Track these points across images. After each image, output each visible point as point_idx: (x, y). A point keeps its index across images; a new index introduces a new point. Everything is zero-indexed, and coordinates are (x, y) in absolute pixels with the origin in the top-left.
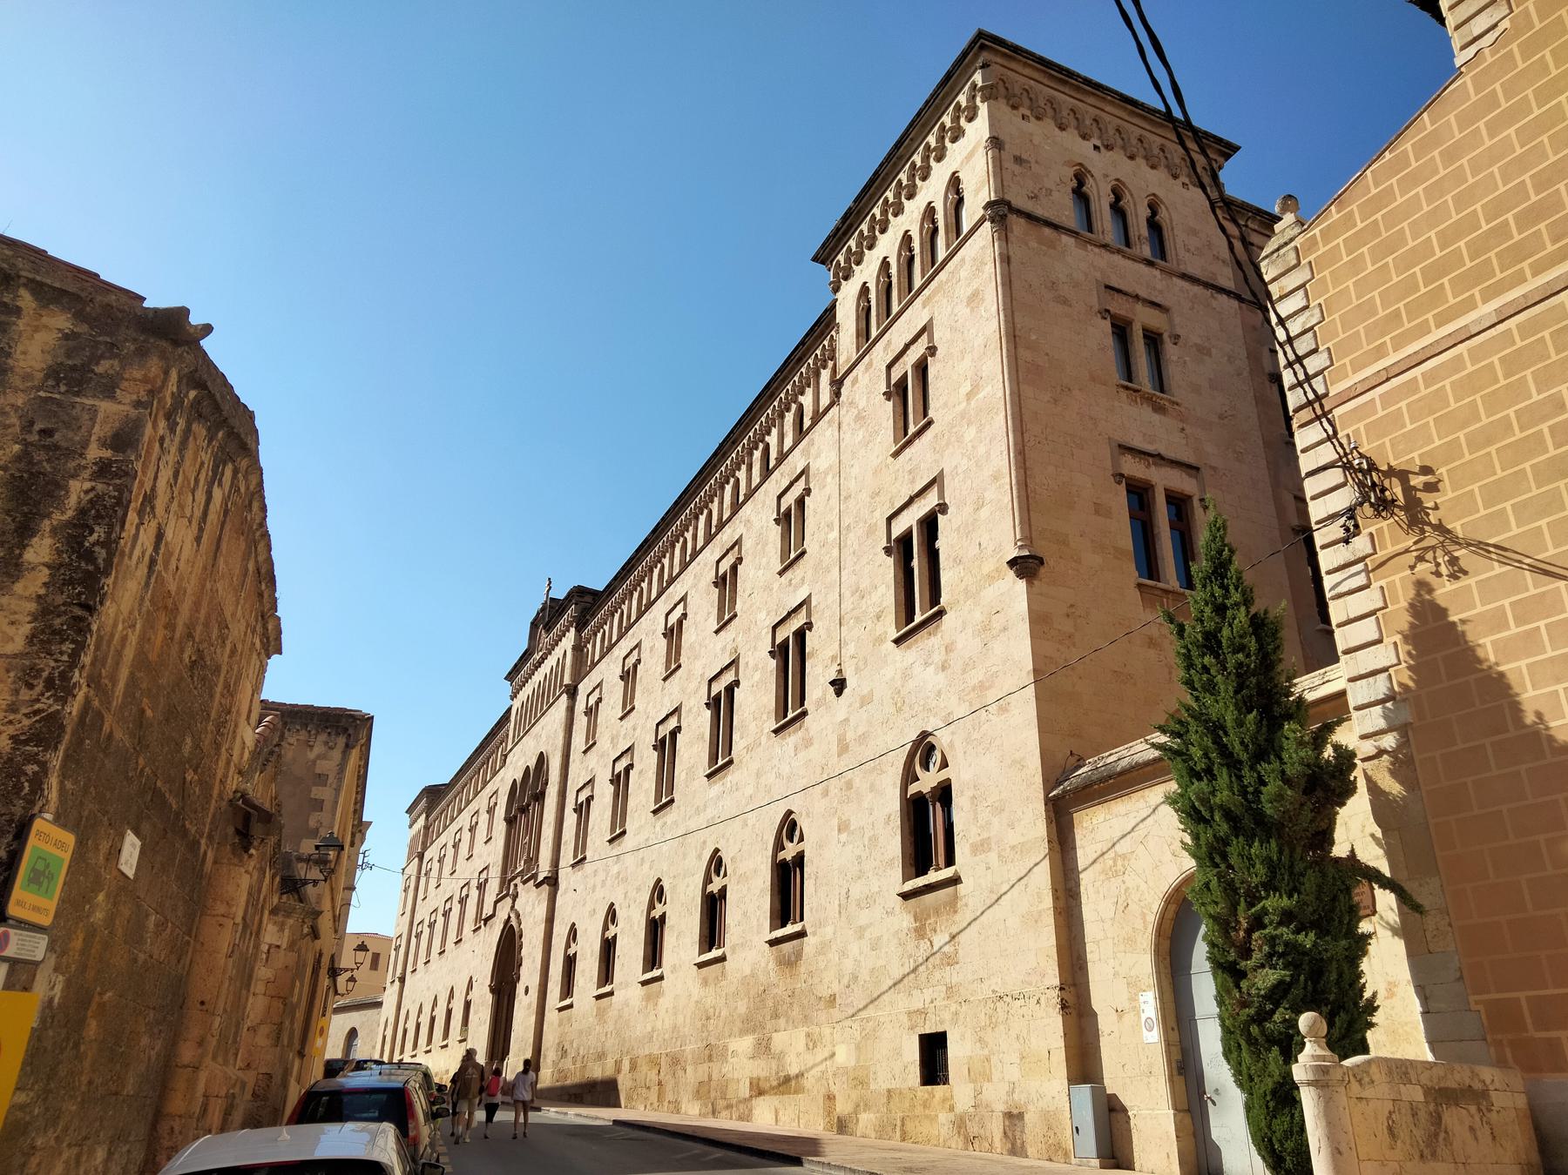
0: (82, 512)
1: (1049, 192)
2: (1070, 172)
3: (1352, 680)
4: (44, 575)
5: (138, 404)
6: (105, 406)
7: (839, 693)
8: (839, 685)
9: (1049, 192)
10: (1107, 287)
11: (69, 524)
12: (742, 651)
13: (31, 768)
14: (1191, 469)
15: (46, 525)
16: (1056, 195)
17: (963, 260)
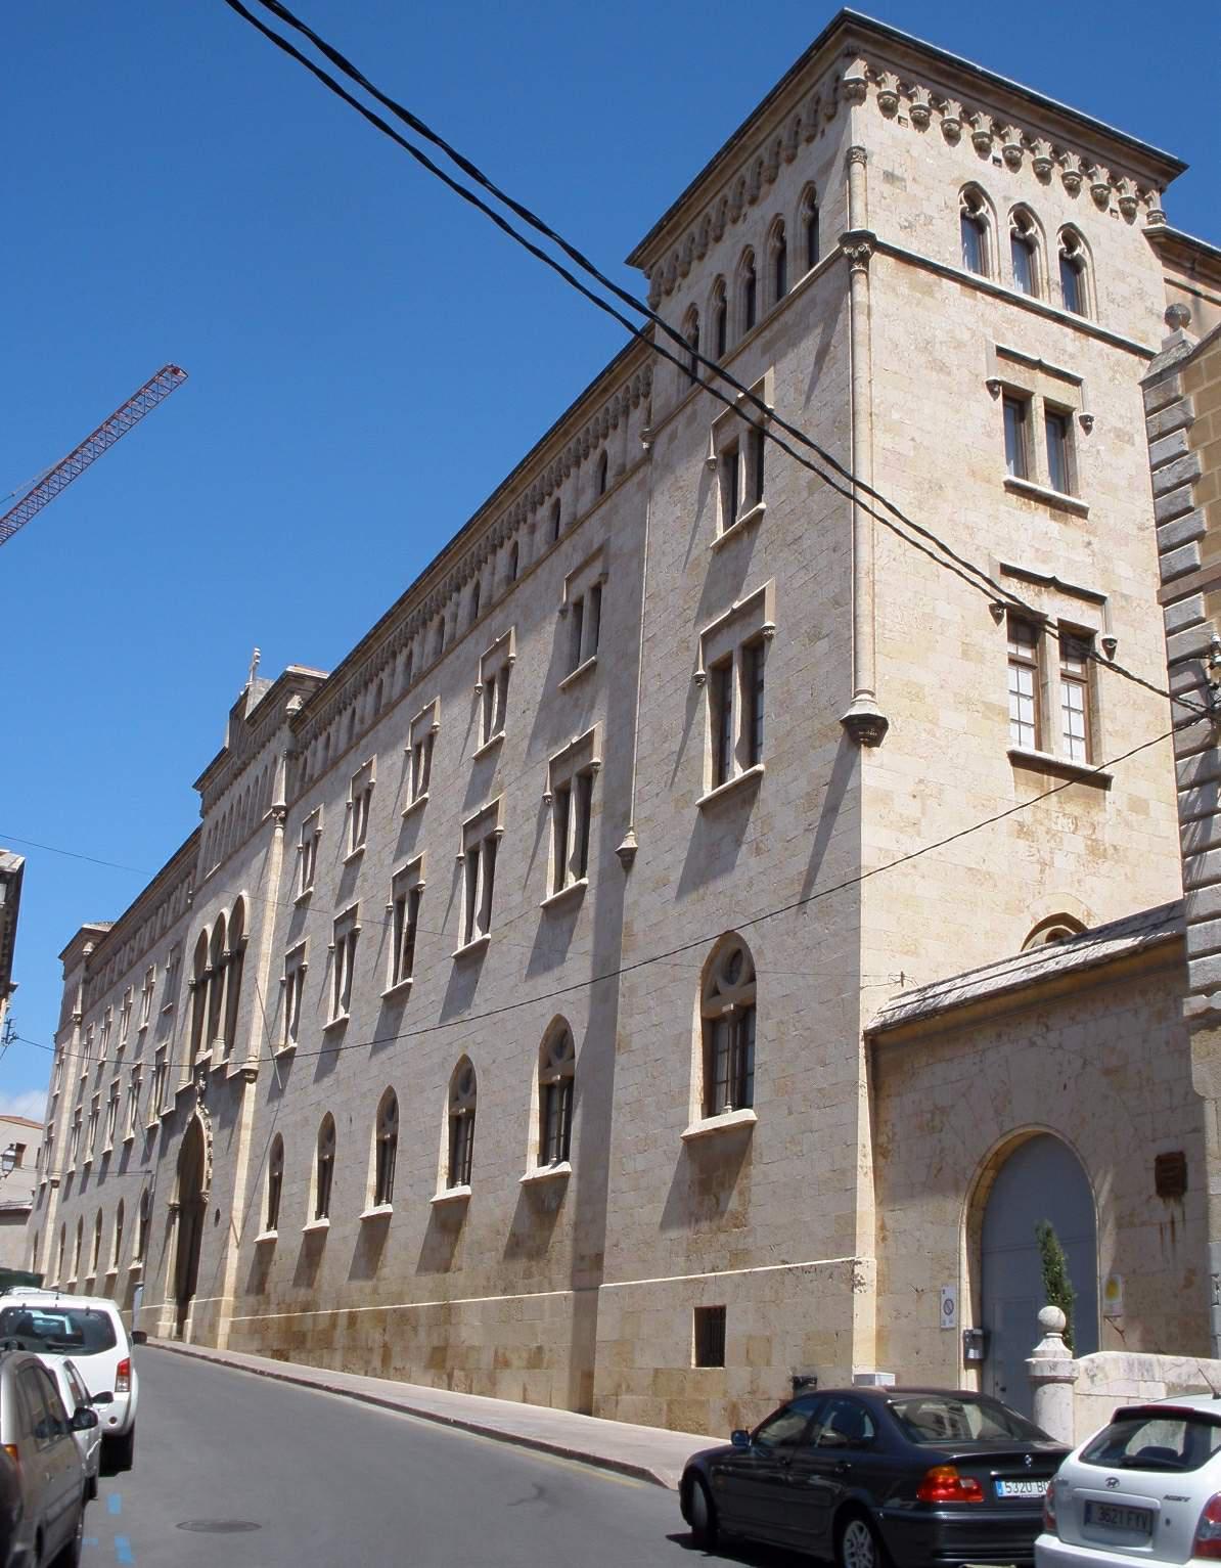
1: (929, 220)
9: (929, 220)
14: (1096, 600)
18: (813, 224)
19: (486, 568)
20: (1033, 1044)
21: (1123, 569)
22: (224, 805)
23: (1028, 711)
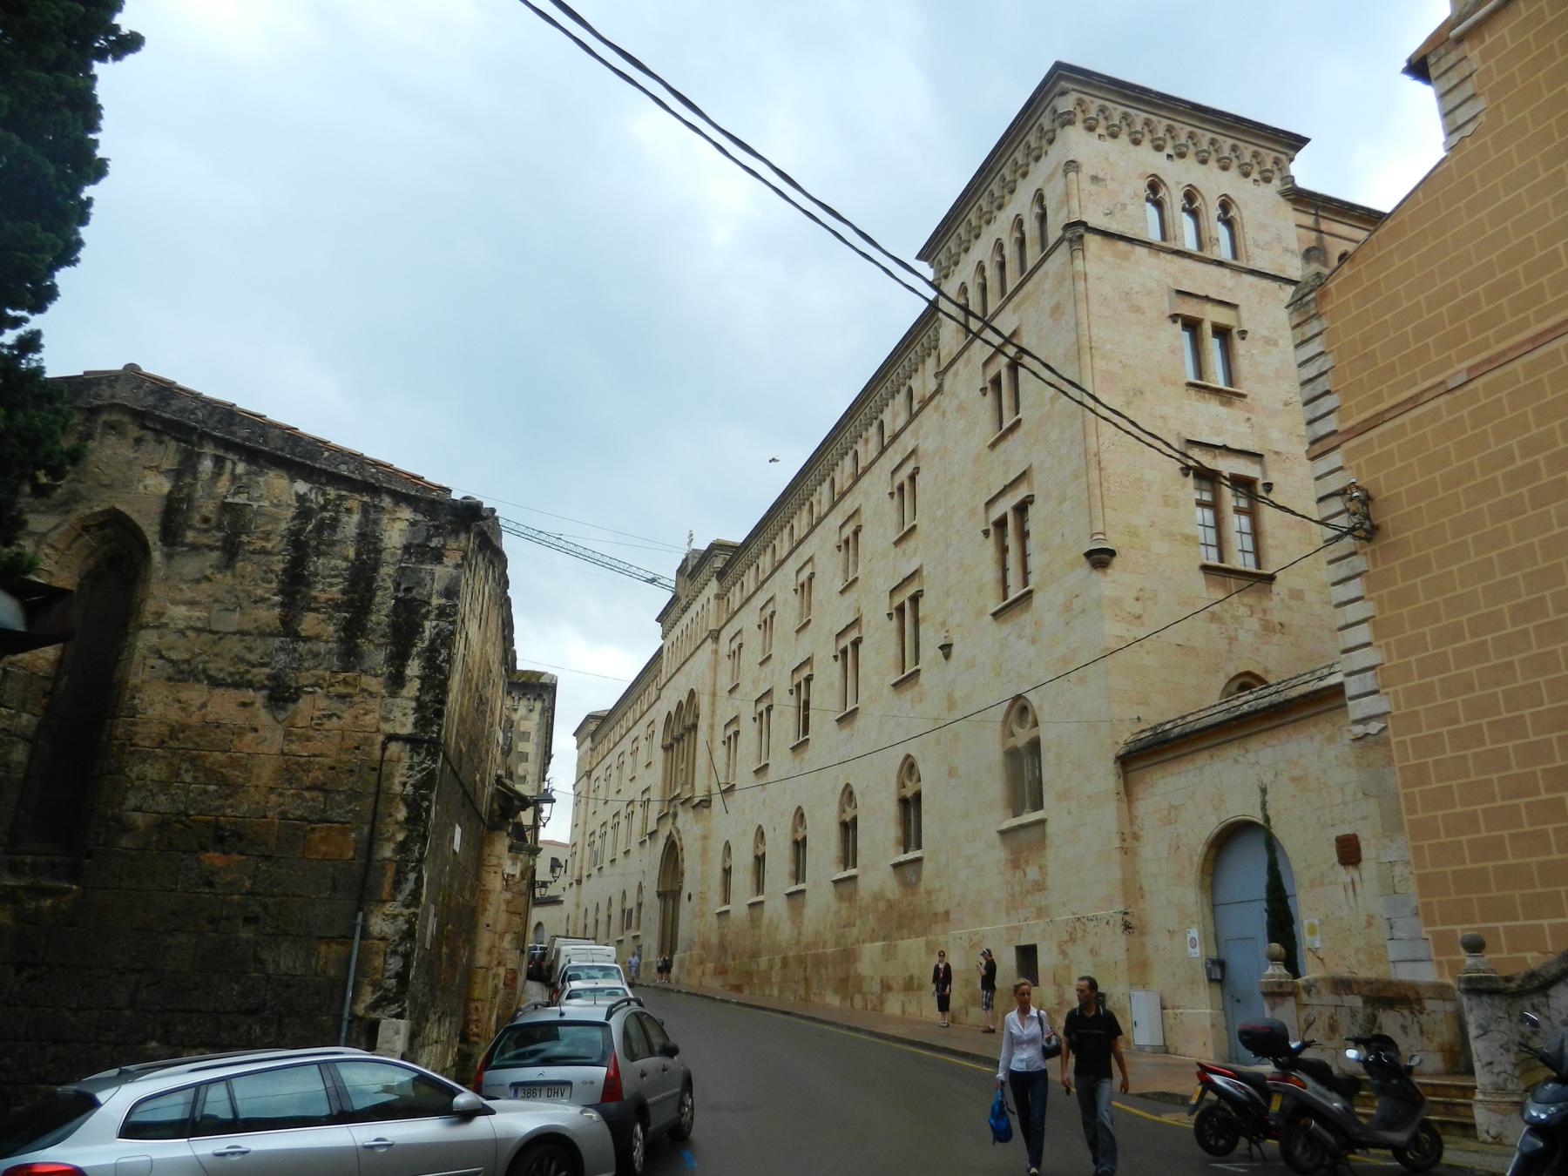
0: (432, 641)
1: (1124, 206)
2: (1144, 184)
3: (1348, 675)
4: (417, 683)
5: (457, 566)
6: (439, 570)
7: (947, 656)
8: (946, 649)
9: (1124, 206)
10: (1179, 292)
11: (427, 649)
12: (864, 611)
13: (426, 804)
14: (1256, 456)
15: (415, 650)
16: (1130, 207)
17: (1046, 273)
18: (1042, 218)
19: (838, 470)
20: (1236, 761)
21: (1274, 434)
22: (677, 631)
23: (1211, 536)
